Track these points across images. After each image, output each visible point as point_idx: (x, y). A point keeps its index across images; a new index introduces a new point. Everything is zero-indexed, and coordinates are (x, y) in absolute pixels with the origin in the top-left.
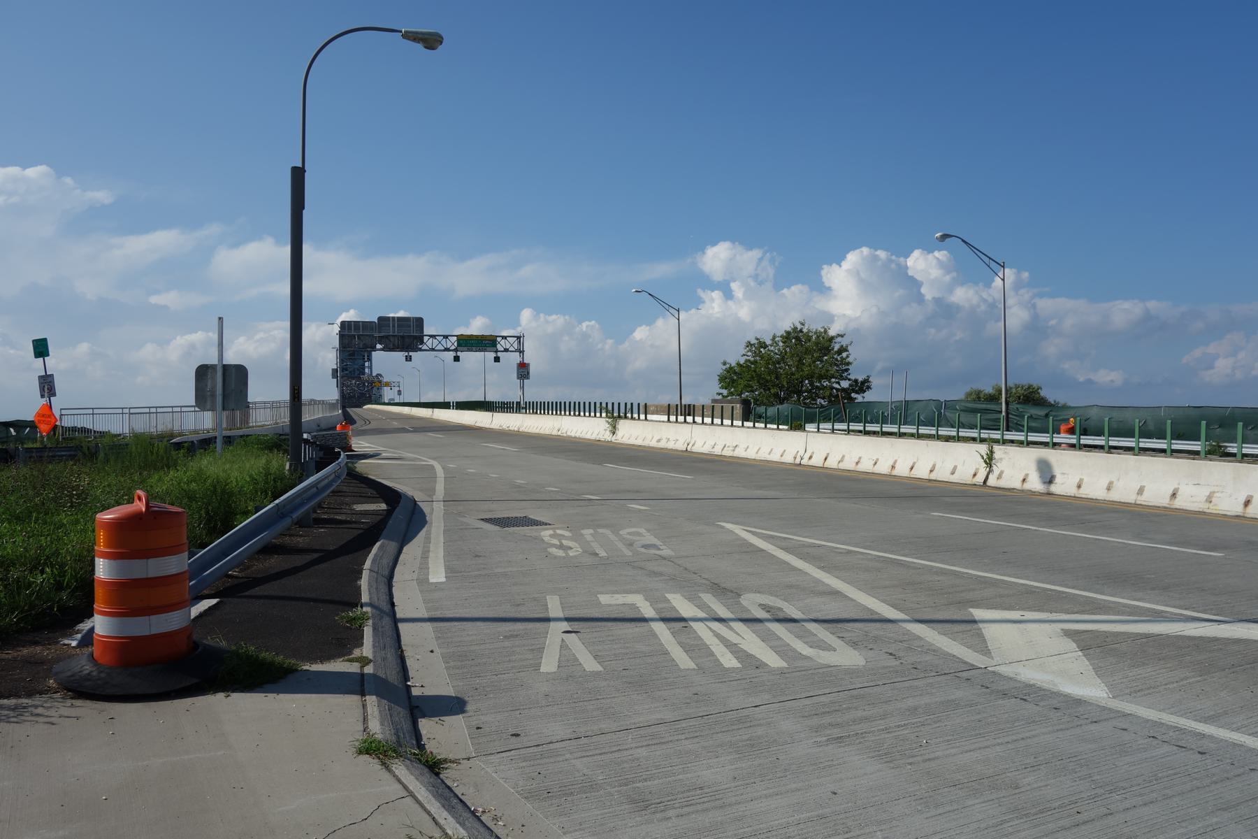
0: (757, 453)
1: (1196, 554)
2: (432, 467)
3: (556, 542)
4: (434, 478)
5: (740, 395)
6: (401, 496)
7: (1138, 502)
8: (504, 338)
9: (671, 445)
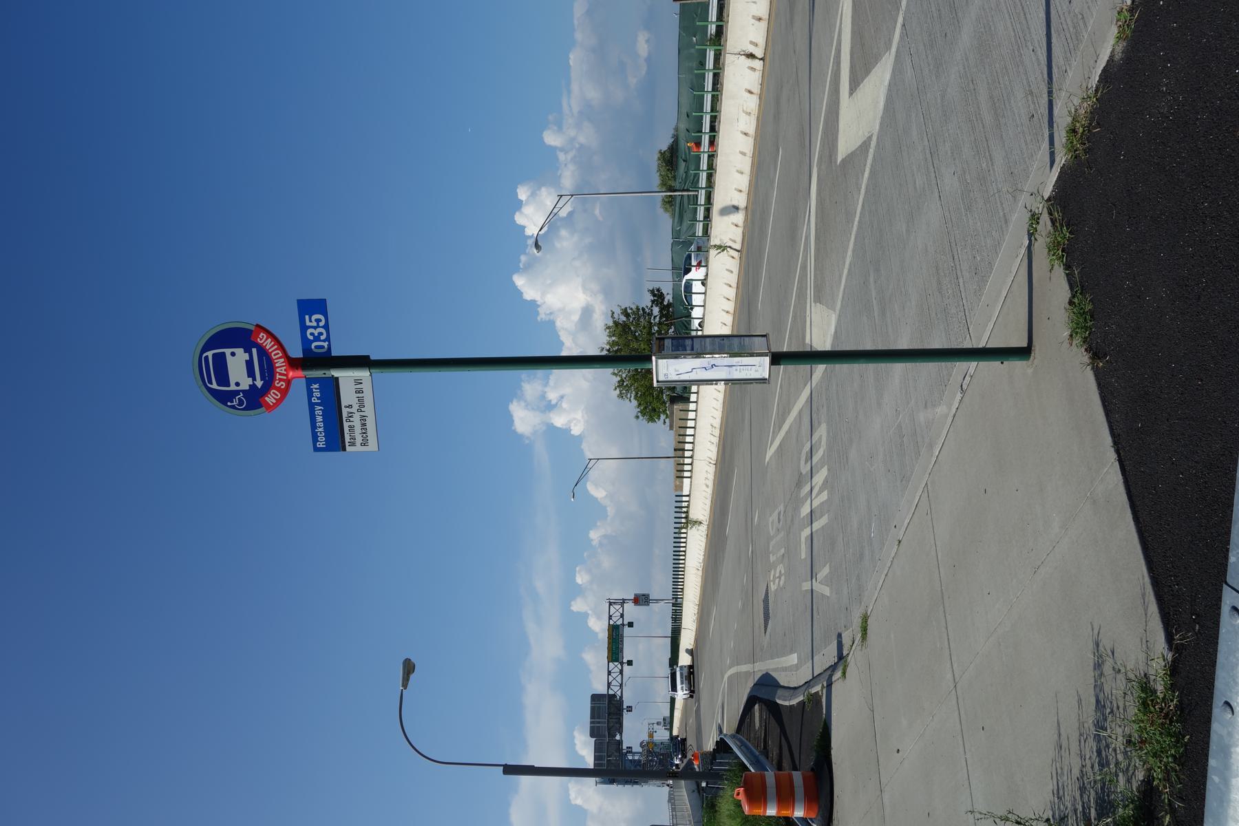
0: (717, 410)
1: (773, 215)
3: (777, 580)
4: (738, 674)
5: (664, 403)
7: (751, 156)
8: (610, 618)
9: (711, 477)
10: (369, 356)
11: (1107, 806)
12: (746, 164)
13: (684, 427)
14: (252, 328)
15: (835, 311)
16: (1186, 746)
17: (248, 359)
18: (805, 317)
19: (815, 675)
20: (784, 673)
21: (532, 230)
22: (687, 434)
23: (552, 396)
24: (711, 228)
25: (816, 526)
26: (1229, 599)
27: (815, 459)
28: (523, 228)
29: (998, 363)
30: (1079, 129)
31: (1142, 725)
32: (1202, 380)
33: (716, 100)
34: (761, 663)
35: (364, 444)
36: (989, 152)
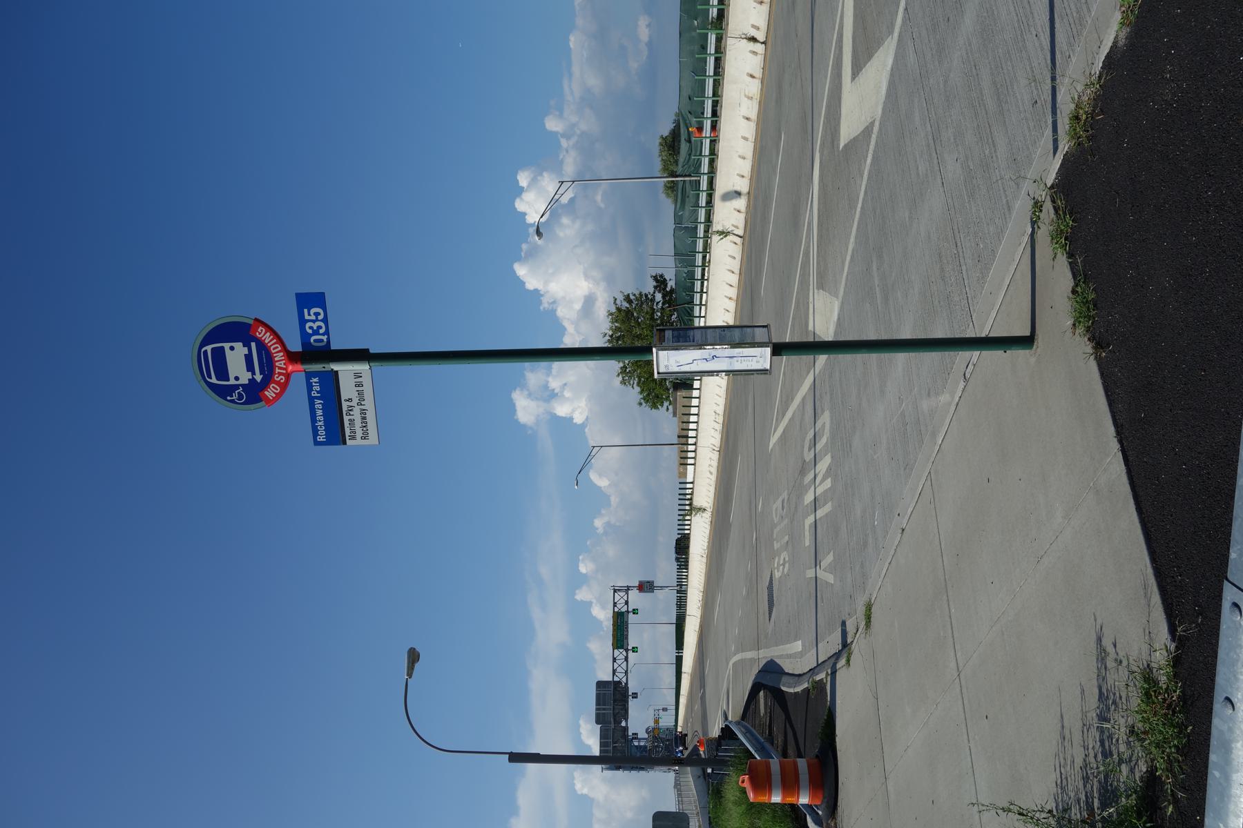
2: (733, 664)
4: (742, 661)
6: (756, 683)
7: (753, 141)
8: (615, 604)
9: (715, 464)
10: (368, 350)
11: (1110, 796)
12: (748, 149)
13: (685, 451)
14: (251, 322)
15: (837, 297)
16: (1189, 737)
17: (247, 353)
18: (808, 303)
19: (819, 663)
20: (789, 660)
21: (533, 218)
22: (691, 420)
23: (554, 384)
24: (713, 214)
25: (820, 513)
26: (1229, 594)
27: (819, 446)
28: (524, 214)
29: (1000, 352)
30: (1082, 115)
31: (1145, 715)
32: (1205, 371)
33: (717, 85)
34: (765, 650)
35: (364, 438)
36: (992, 138)
